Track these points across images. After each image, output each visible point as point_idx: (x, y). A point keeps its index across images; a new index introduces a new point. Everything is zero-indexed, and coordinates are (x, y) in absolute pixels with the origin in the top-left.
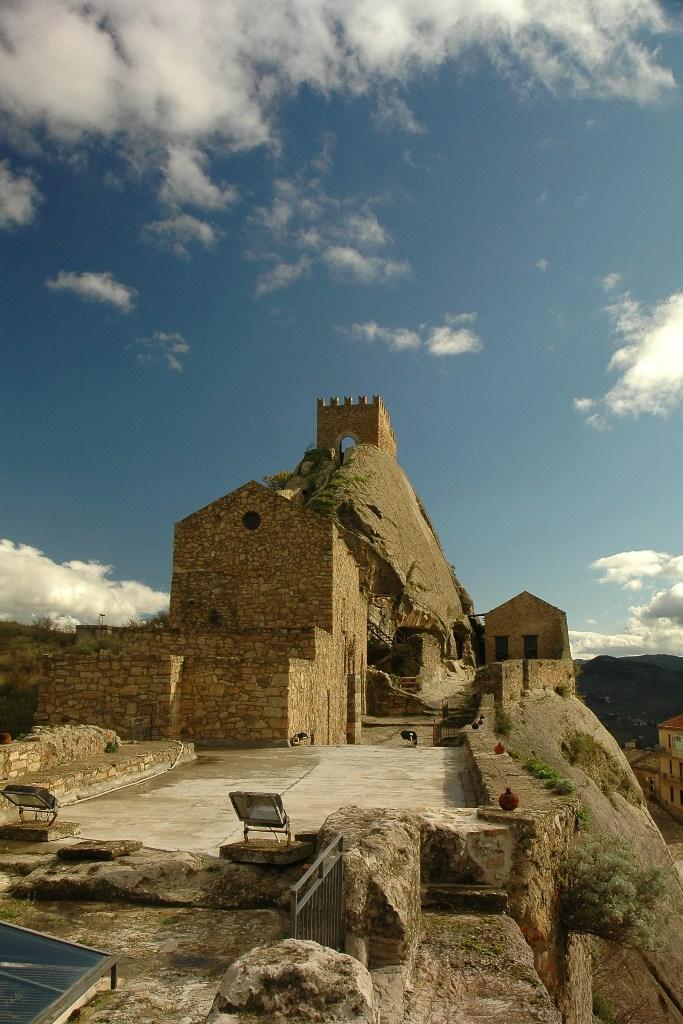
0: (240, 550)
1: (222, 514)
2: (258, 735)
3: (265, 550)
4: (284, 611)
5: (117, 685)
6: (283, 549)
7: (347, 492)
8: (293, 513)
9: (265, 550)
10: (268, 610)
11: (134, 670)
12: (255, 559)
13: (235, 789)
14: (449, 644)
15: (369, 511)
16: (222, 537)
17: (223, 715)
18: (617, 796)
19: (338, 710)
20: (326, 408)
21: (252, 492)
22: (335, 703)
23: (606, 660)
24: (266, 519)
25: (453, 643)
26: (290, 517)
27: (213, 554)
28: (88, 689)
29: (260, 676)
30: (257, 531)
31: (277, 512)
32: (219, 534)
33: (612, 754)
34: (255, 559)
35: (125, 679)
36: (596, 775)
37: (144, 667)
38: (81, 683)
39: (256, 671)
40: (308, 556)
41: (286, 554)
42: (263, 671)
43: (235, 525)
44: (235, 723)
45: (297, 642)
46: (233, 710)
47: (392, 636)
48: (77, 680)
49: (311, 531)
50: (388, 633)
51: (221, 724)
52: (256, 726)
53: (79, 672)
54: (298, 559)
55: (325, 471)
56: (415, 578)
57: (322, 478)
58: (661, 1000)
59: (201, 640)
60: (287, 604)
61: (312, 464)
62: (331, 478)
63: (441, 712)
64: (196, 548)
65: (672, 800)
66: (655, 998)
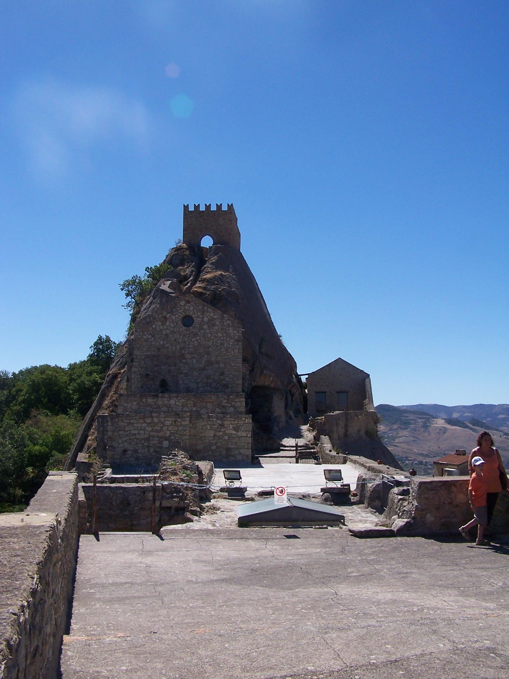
1: (168, 316)
2: (233, 458)
3: (197, 340)
5: (157, 431)
8: (215, 317)
9: (197, 340)
11: (168, 423)
12: (190, 346)
13: (325, 469)
16: (168, 332)
17: (214, 447)
26: (213, 319)
27: (162, 342)
28: (139, 433)
29: (235, 426)
30: (191, 328)
32: (165, 329)
35: (162, 428)
36: (299, 547)
37: (172, 421)
38: (135, 430)
43: (177, 323)
45: (233, 403)
48: (132, 428)
49: (227, 329)
53: (133, 423)
56: (263, 350)
59: (172, 402)
60: (212, 377)
63: (293, 454)
64: (150, 339)
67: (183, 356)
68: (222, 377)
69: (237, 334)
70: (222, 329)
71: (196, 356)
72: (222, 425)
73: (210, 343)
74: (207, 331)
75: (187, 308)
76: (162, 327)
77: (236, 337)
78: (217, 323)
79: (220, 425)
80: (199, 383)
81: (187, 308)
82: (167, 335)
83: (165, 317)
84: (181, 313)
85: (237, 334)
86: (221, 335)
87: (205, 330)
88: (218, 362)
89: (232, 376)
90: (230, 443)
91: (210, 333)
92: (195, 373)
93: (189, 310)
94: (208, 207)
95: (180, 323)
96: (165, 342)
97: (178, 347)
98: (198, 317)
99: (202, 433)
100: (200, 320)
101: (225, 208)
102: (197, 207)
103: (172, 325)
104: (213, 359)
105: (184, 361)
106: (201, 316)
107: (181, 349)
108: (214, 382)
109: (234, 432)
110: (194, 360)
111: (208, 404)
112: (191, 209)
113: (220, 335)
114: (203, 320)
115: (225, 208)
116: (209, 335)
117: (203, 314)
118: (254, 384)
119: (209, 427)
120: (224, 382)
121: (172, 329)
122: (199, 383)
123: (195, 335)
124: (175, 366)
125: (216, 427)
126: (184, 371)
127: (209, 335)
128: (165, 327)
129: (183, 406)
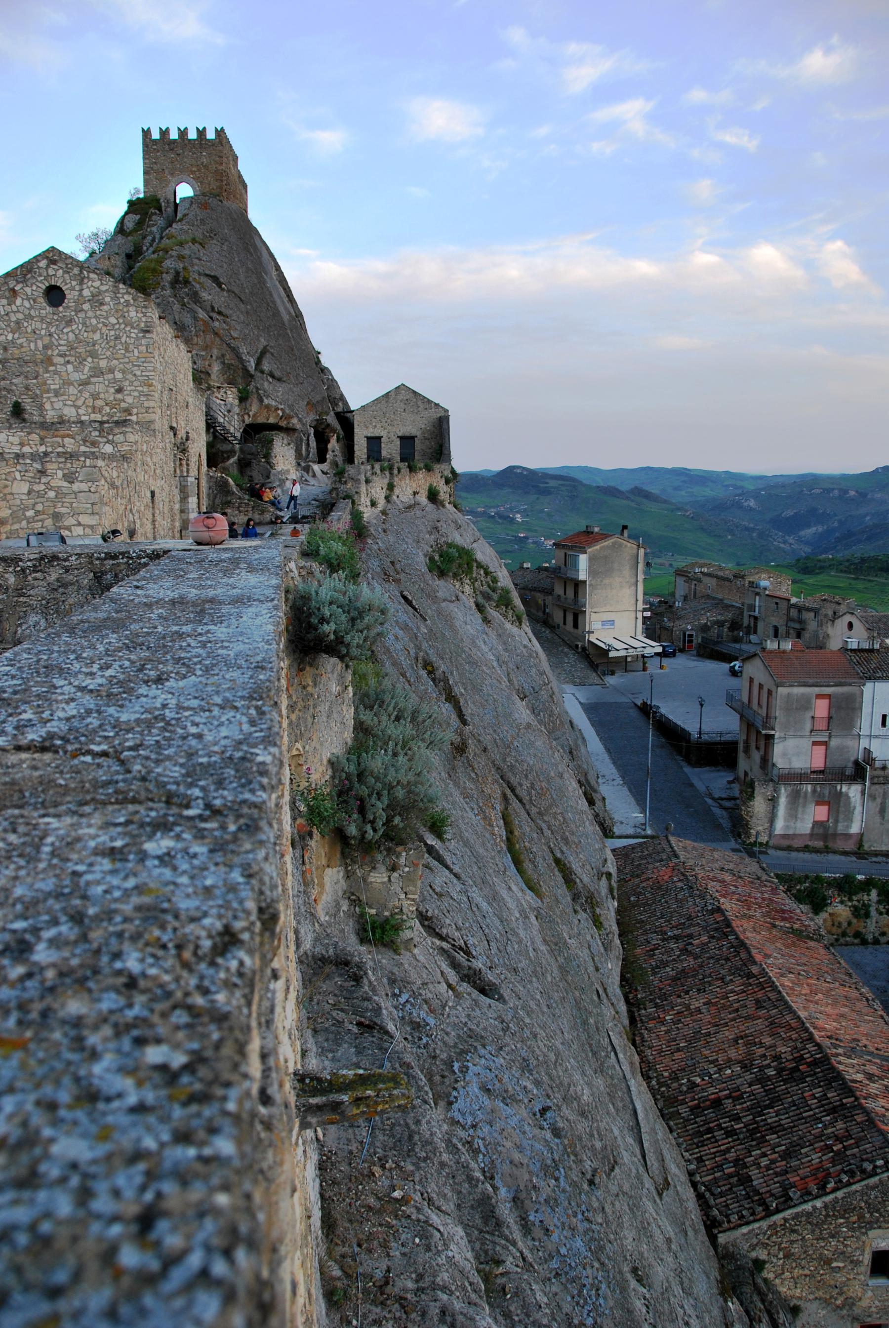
0: (43, 332)
3: (72, 331)
4: (99, 403)
6: (94, 332)
7: (181, 257)
8: (104, 288)
10: (80, 403)
12: (62, 342)
14: (308, 445)
15: (209, 282)
16: (20, 316)
18: (493, 613)
19: (167, 514)
20: (155, 142)
21: (53, 262)
22: (162, 505)
23: (519, 471)
24: (71, 296)
25: (313, 444)
26: (100, 293)
27: (10, 337)
29: (66, 471)
30: (61, 309)
31: (85, 286)
32: (15, 312)
33: (491, 569)
34: (62, 342)
39: (61, 465)
40: (123, 340)
41: (97, 336)
42: (69, 465)
43: (35, 301)
44: (42, 521)
45: (111, 437)
46: (39, 507)
47: (238, 435)
50: (234, 427)
51: (28, 523)
52: (66, 523)
54: (112, 344)
55: (154, 229)
56: (266, 367)
57: (149, 238)
58: (505, 797)
60: (102, 396)
61: (138, 217)
62: (161, 238)
65: (565, 623)
66: (498, 794)
67: (49, 361)
68: (119, 396)
69: (144, 319)
70: (117, 311)
71: (72, 359)
72: (43, 472)
73: (97, 336)
74: (90, 314)
75: (51, 272)
76: (8, 308)
77: (143, 325)
78: (107, 299)
79: (39, 471)
80: (79, 407)
81: (51, 272)
82: (18, 322)
83: (13, 291)
84: (41, 282)
85: (144, 319)
86: (115, 321)
87: (86, 312)
88: (111, 371)
89: (136, 394)
90: (60, 505)
91: (96, 317)
92: (72, 390)
93: (55, 275)
94: (183, 133)
95: (41, 300)
96: (16, 336)
97: (40, 344)
98: (73, 289)
99: (6, 486)
100: (77, 293)
101: (211, 135)
102: (165, 133)
103: (27, 304)
104: (103, 364)
105: (52, 368)
106: (77, 288)
107: (46, 347)
108: (107, 404)
109: (66, 484)
110: (70, 368)
111: (67, 440)
112: (156, 135)
113: (113, 320)
114: (81, 295)
115: (211, 135)
116: (94, 321)
117: (81, 283)
118: (248, 420)
119: (18, 477)
120: (123, 405)
121: (27, 312)
122: (79, 407)
123: (69, 322)
124: (36, 378)
125: (31, 474)
126: (52, 387)
127: (94, 321)
128: (14, 308)
129: (22, 444)
